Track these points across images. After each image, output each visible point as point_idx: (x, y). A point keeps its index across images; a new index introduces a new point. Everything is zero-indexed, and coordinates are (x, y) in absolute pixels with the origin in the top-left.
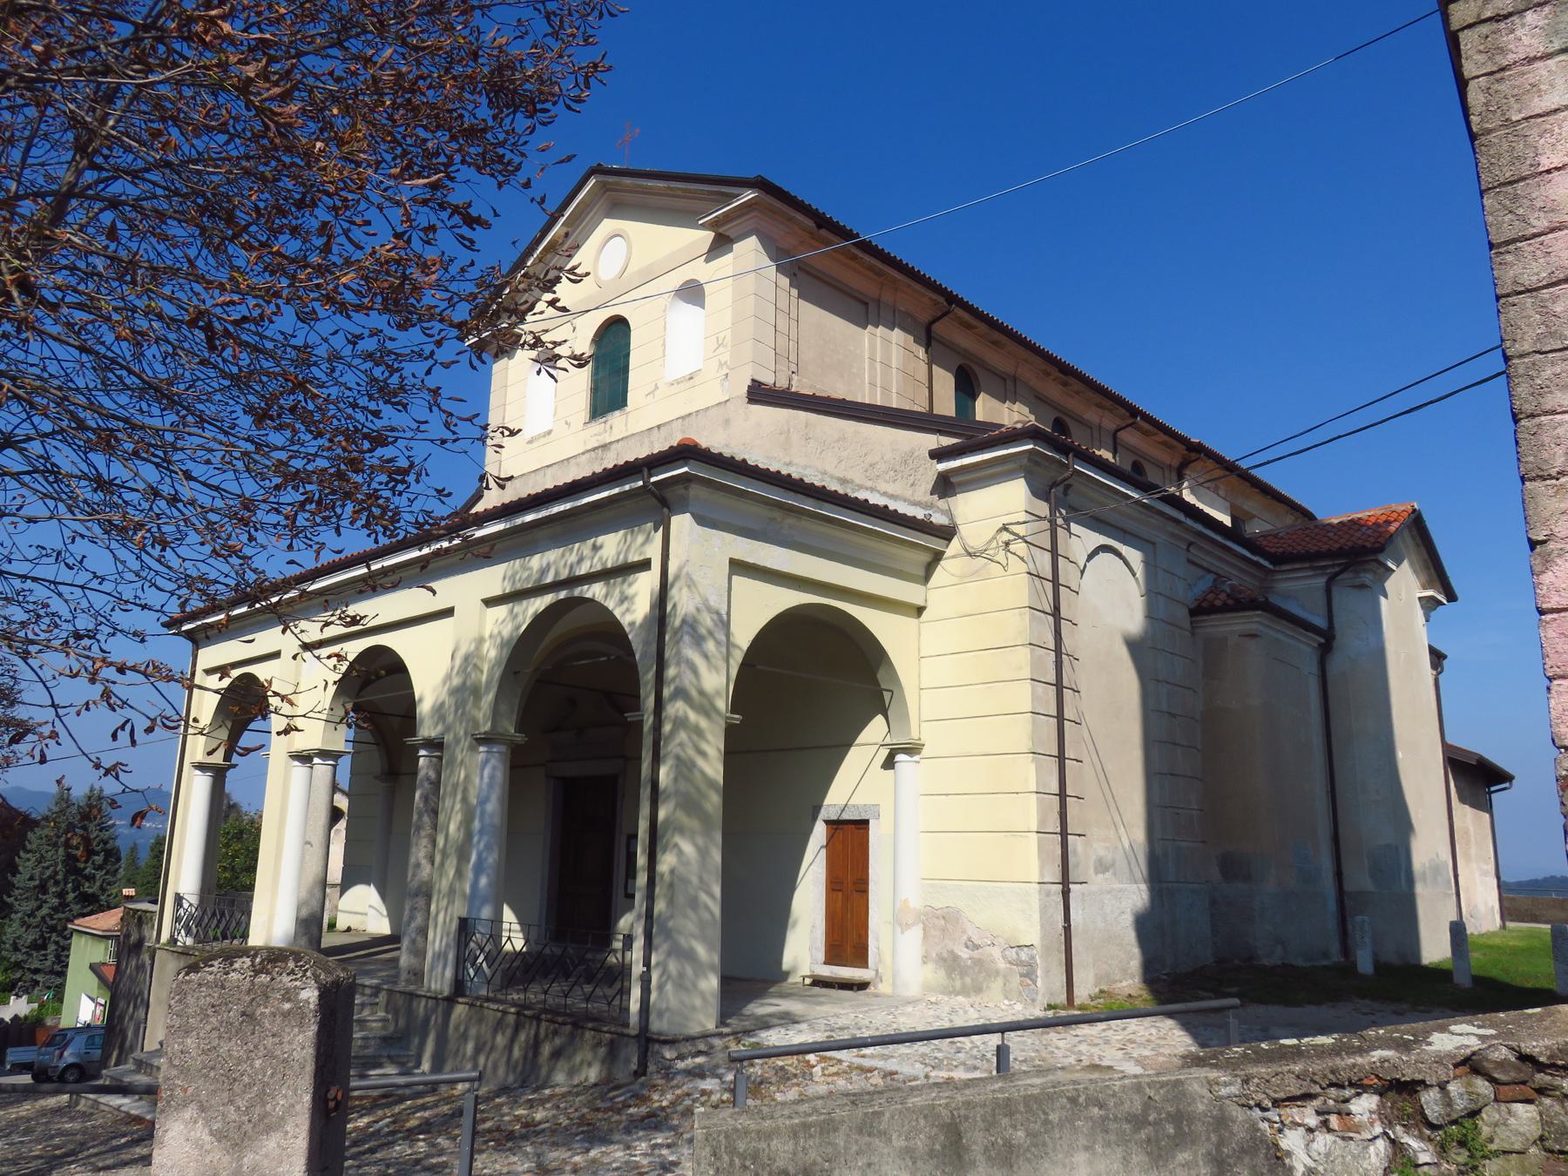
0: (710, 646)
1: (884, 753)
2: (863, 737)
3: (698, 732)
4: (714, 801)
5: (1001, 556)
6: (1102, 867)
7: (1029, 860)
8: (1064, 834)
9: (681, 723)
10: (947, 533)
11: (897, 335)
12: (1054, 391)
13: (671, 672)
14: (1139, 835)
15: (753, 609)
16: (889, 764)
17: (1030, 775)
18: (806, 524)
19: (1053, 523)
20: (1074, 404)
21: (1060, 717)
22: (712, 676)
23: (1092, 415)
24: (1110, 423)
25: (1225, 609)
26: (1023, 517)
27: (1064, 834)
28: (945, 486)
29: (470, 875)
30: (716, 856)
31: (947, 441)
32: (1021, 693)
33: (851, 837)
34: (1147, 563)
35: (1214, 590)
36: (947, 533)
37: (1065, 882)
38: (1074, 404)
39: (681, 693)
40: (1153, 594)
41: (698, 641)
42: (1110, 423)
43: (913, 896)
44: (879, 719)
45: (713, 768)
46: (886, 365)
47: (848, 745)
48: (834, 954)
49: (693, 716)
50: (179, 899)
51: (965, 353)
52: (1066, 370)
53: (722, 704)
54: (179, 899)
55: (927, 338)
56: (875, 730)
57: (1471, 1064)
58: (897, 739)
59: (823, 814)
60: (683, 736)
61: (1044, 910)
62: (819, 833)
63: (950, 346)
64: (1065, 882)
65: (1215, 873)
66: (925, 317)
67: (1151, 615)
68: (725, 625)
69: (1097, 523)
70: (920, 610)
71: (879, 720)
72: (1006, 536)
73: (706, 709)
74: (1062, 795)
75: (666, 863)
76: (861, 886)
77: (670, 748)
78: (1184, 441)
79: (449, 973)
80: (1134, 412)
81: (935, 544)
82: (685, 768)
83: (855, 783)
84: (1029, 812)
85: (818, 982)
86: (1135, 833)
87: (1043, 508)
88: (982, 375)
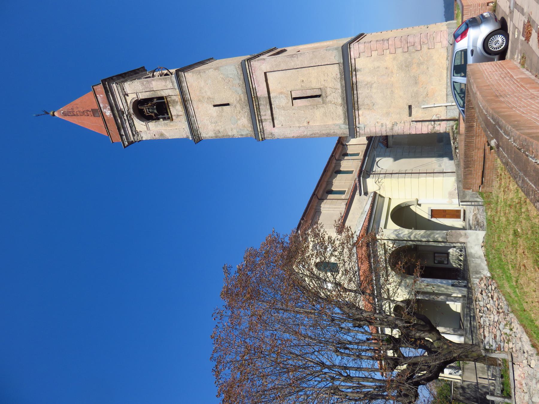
0: (400, 232)
1: (418, 206)
2: (414, 210)
3: (416, 234)
4: (429, 232)
5: (381, 183)
6: (440, 166)
7: (439, 179)
8: (434, 173)
9: (415, 237)
10: (375, 193)
11: (322, 205)
12: (329, 174)
13: (406, 239)
14: (434, 159)
15: (392, 226)
16: (420, 205)
17: (423, 179)
18: (376, 217)
19: (374, 174)
20: (331, 169)
21: (405, 173)
22: (405, 232)
23: (333, 165)
24: (335, 161)
25: (387, 141)
26: (374, 179)
27: (434, 173)
28: (366, 194)
29: (443, 285)
30: (439, 231)
31: (358, 191)
32: (408, 180)
33: (435, 213)
34: (379, 157)
35: (382, 143)
36: (375, 193)
37: (443, 173)
38: (331, 169)
39: (409, 237)
40: (385, 156)
41: (399, 234)
42: (335, 161)
43: (447, 200)
44: (411, 207)
45: (422, 232)
46: (329, 208)
47: (416, 213)
48: (458, 217)
49: (413, 235)
50: (450, 374)
51: (323, 192)
52: (325, 171)
53: (411, 230)
54: (450, 374)
55: (322, 199)
56: (413, 208)
57: (454, 143)
58: (416, 203)
59: (430, 219)
60: (417, 236)
61: (448, 177)
62: (434, 220)
63: (322, 195)
64: (443, 173)
65: (442, 144)
66: (317, 200)
67: (389, 156)
68: (396, 230)
69: (372, 166)
70: (390, 199)
71: (411, 207)
72: (377, 182)
73: (412, 233)
74: (426, 173)
75: (440, 239)
76: (444, 211)
77: (419, 239)
78: (337, 144)
79: (463, 289)
80: (332, 156)
81: (377, 196)
82: (422, 236)
83: (424, 212)
84: (430, 179)
85: (464, 220)
86: (433, 160)
87: (371, 176)
88: (328, 189)
